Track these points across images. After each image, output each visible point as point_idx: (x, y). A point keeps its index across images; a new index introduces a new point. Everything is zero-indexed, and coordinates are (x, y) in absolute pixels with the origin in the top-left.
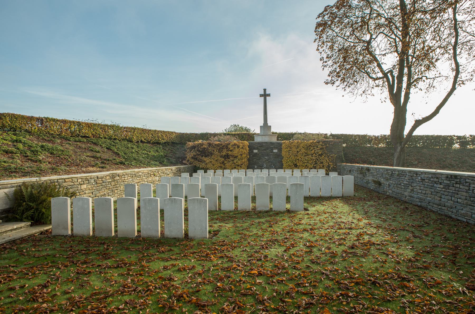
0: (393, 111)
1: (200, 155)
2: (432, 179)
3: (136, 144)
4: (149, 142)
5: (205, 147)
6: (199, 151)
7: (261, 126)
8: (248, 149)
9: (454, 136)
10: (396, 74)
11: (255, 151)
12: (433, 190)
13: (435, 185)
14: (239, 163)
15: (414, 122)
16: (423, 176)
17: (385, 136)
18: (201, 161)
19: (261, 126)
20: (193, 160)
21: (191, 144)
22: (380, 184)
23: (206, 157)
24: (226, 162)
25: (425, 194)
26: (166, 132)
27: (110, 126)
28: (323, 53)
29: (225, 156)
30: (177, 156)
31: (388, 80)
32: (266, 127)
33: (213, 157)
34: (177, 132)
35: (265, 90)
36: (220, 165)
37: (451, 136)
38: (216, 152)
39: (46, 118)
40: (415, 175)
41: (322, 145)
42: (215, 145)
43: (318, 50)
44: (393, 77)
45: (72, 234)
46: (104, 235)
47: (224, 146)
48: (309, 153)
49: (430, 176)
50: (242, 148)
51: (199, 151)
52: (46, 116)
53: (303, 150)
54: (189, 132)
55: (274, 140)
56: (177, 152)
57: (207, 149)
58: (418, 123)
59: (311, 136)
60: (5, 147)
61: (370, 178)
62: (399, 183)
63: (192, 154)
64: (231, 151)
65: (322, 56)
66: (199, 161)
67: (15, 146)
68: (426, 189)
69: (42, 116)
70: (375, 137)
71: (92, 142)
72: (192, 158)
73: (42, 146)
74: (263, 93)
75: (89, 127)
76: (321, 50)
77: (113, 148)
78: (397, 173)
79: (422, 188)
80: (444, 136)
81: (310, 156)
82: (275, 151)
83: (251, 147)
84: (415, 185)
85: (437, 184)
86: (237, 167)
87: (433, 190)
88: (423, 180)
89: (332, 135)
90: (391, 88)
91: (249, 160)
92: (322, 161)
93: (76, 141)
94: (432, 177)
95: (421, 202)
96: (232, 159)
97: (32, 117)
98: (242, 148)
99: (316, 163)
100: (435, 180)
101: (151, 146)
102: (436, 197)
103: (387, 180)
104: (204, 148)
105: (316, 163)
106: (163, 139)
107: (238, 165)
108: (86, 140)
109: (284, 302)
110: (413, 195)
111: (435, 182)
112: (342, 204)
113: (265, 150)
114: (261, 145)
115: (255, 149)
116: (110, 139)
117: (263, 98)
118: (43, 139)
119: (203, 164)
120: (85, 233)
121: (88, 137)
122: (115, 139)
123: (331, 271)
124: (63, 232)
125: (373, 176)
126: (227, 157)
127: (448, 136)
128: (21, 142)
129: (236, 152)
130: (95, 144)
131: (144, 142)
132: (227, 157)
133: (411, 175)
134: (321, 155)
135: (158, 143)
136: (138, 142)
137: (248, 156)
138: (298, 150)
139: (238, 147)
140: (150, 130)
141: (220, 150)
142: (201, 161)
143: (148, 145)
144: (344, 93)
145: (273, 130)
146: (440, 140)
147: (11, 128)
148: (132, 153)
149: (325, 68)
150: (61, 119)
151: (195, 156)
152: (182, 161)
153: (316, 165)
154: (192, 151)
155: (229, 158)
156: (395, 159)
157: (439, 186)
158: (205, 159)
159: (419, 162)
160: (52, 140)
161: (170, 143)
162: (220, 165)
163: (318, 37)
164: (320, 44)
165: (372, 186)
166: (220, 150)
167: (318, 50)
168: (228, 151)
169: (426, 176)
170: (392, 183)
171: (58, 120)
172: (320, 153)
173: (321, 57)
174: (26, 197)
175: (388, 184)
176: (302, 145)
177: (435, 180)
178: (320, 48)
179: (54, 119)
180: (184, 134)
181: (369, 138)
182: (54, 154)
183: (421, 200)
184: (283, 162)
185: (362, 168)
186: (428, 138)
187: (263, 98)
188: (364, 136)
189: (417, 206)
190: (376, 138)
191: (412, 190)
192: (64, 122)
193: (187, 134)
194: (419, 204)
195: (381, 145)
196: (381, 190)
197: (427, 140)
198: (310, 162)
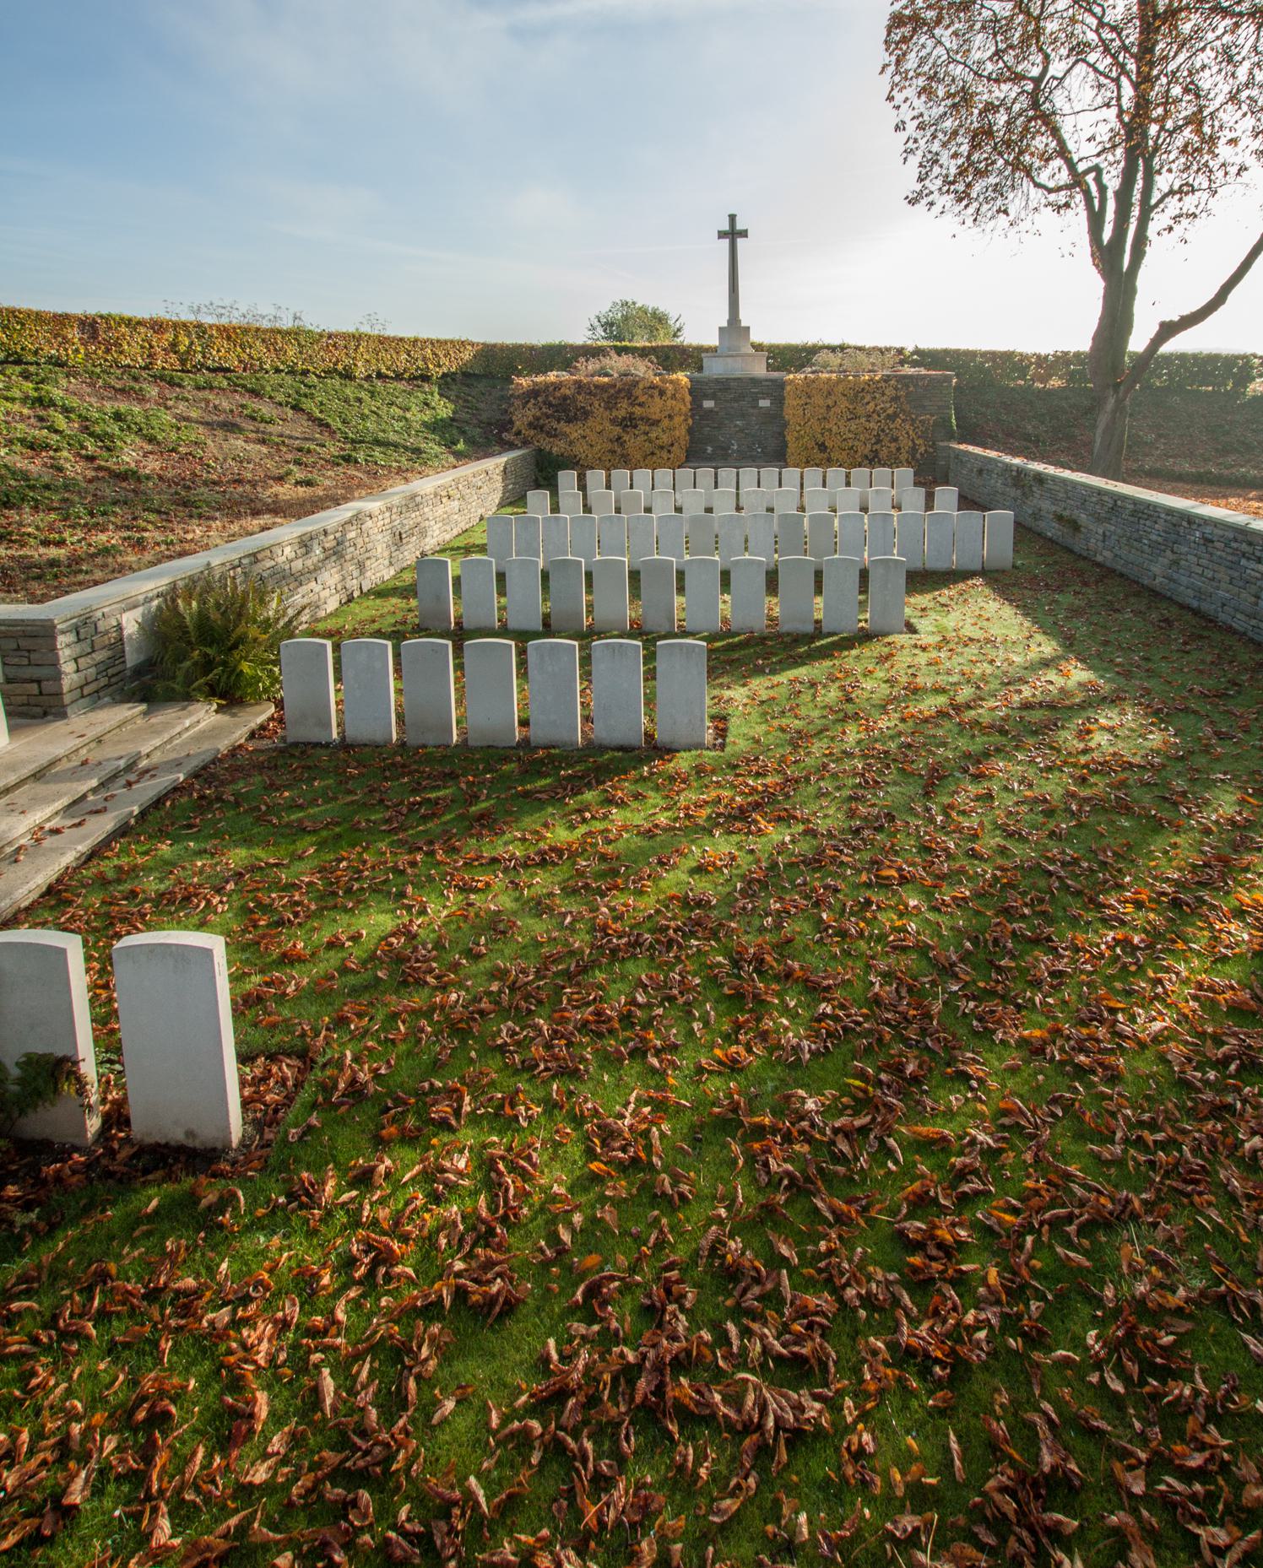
0: (1101, 292)
1: (551, 416)
2: (1234, 545)
3: (366, 385)
4: (399, 377)
5: (568, 392)
6: (550, 405)
7: (721, 329)
8: (688, 398)
9: (1255, 356)
10: (1113, 182)
11: (708, 404)
12: (1236, 574)
13: (1243, 562)
14: (665, 439)
15: (1157, 328)
16: (1208, 530)
17: (1066, 353)
18: (553, 434)
19: (721, 329)
20: (532, 432)
21: (524, 382)
22: (1075, 526)
23: (569, 421)
24: (626, 438)
25: (1213, 579)
26: (446, 342)
27: (288, 333)
28: (904, 107)
29: (624, 419)
30: (484, 417)
31: (1087, 194)
32: (734, 328)
33: (590, 423)
34: (475, 340)
35: (732, 218)
36: (609, 446)
37: (1245, 357)
38: (598, 407)
39: (106, 318)
40: (1185, 524)
41: (896, 389)
42: (596, 387)
43: (890, 98)
44: (1102, 189)
45: (343, 738)
46: (431, 739)
47: (620, 391)
48: (860, 410)
49: (1231, 536)
50: (674, 397)
51: (550, 405)
52: (104, 312)
53: (844, 404)
54: (510, 340)
55: (759, 370)
56: (482, 406)
57: (574, 400)
58: (1168, 330)
59: (861, 356)
60: (21, 429)
61: (1046, 505)
62: (1135, 535)
63: (531, 412)
64: (640, 405)
65: (901, 117)
66: (549, 434)
67: (41, 419)
68: (1216, 567)
69: (92, 311)
70: (1039, 356)
71: (244, 386)
72: (531, 425)
73: (118, 417)
74: (726, 227)
75: (229, 338)
76: (899, 97)
77: (308, 404)
78: (1131, 507)
79: (1203, 562)
80: (1226, 357)
81: (863, 420)
82: (764, 403)
83: (698, 391)
84: (1184, 549)
85: (1248, 559)
86: (651, 459)
87: (1236, 574)
88: (1208, 541)
89: (917, 352)
90: (1096, 221)
91: (690, 431)
92: (895, 432)
93: (198, 388)
94: (1236, 540)
95: (1200, 599)
96: (643, 427)
97: (67, 316)
98: (674, 397)
99: (879, 441)
100: (1244, 547)
101: (409, 388)
102: (1244, 595)
103: (1099, 520)
104: (565, 398)
105: (879, 441)
106: (439, 366)
107: (662, 448)
108: (225, 383)
109: (999, 969)
110: (1175, 576)
111: (1244, 555)
112: (996, 605)
113: (735, 400)
114: (723, 386)
115: (706, 397)
116: (292, 372)
117: (726, 242)
118: (107, 386)
119: (562, 444)
120: (378, 737)
121: (227, 370)
122: (305, 373)
123: (1064, 864)
124: (316, 735)
125: (1055, 501)
126: (629, 423)
127: (1238, 357)
128: (55, 405)
129: (656, 408)
130: (255, 393)
131: (387, 377)
132: (629, 423)
133: (1174, 520)
134: (892, 417)
135: (425, 378)
136: (368, 378)
137: (690, 421)
138: (830, 402)
139: (662, 393)
140: (401, 340)
141: (610, 405)
142: (555, 436)
143: (401, 386)
144: (958, 229)
145: (755, 337)
146: (1217, 368)
147: (9, 355)
148: (364, 417)
149: (911, 157)
150: (147, 316)
151: (538, 419)
152: (500, 432)
153: (877, 447)
154: (530, 405)
155: (635, 427)
156: (1099, 432)
157: (1253, 565)
158: (567, 430)
159: (1160, 436)
160: (132, 388)
161: (459, 377)
162: (609, 446)
163: (893, 58)
164: (897, 79)
165: (1052, 530)
166: (610, 405)
167: (890, 98)
168: (632, 404)
169: (1216, 531)
170: (1114, 533)
171: (139, 323)
172: (890, 411)
173: (898, 120)
174: (191, 628)
175: (1101, 531)
176: (840, 388)
177: (1244, 547)
178: (894, 93)
179: (130, 320)
180: (494, 346)
181: (1021, 361)
182: (159, 443)
183: (1200, 594)
184: (788, 438)
185: (1020, 471)
186: (1182, 357)
187: (726, 242)
188: (1009, 355)
189: (1188, 608)
190: (1041, 360)
191: (1176, 563)
192: (158, 326)
193: (504, 348)
194: (1195, 604)
195: (1055, 383)
196: (1079, 546)
197: (1179, 367)
198: (862, 437)
